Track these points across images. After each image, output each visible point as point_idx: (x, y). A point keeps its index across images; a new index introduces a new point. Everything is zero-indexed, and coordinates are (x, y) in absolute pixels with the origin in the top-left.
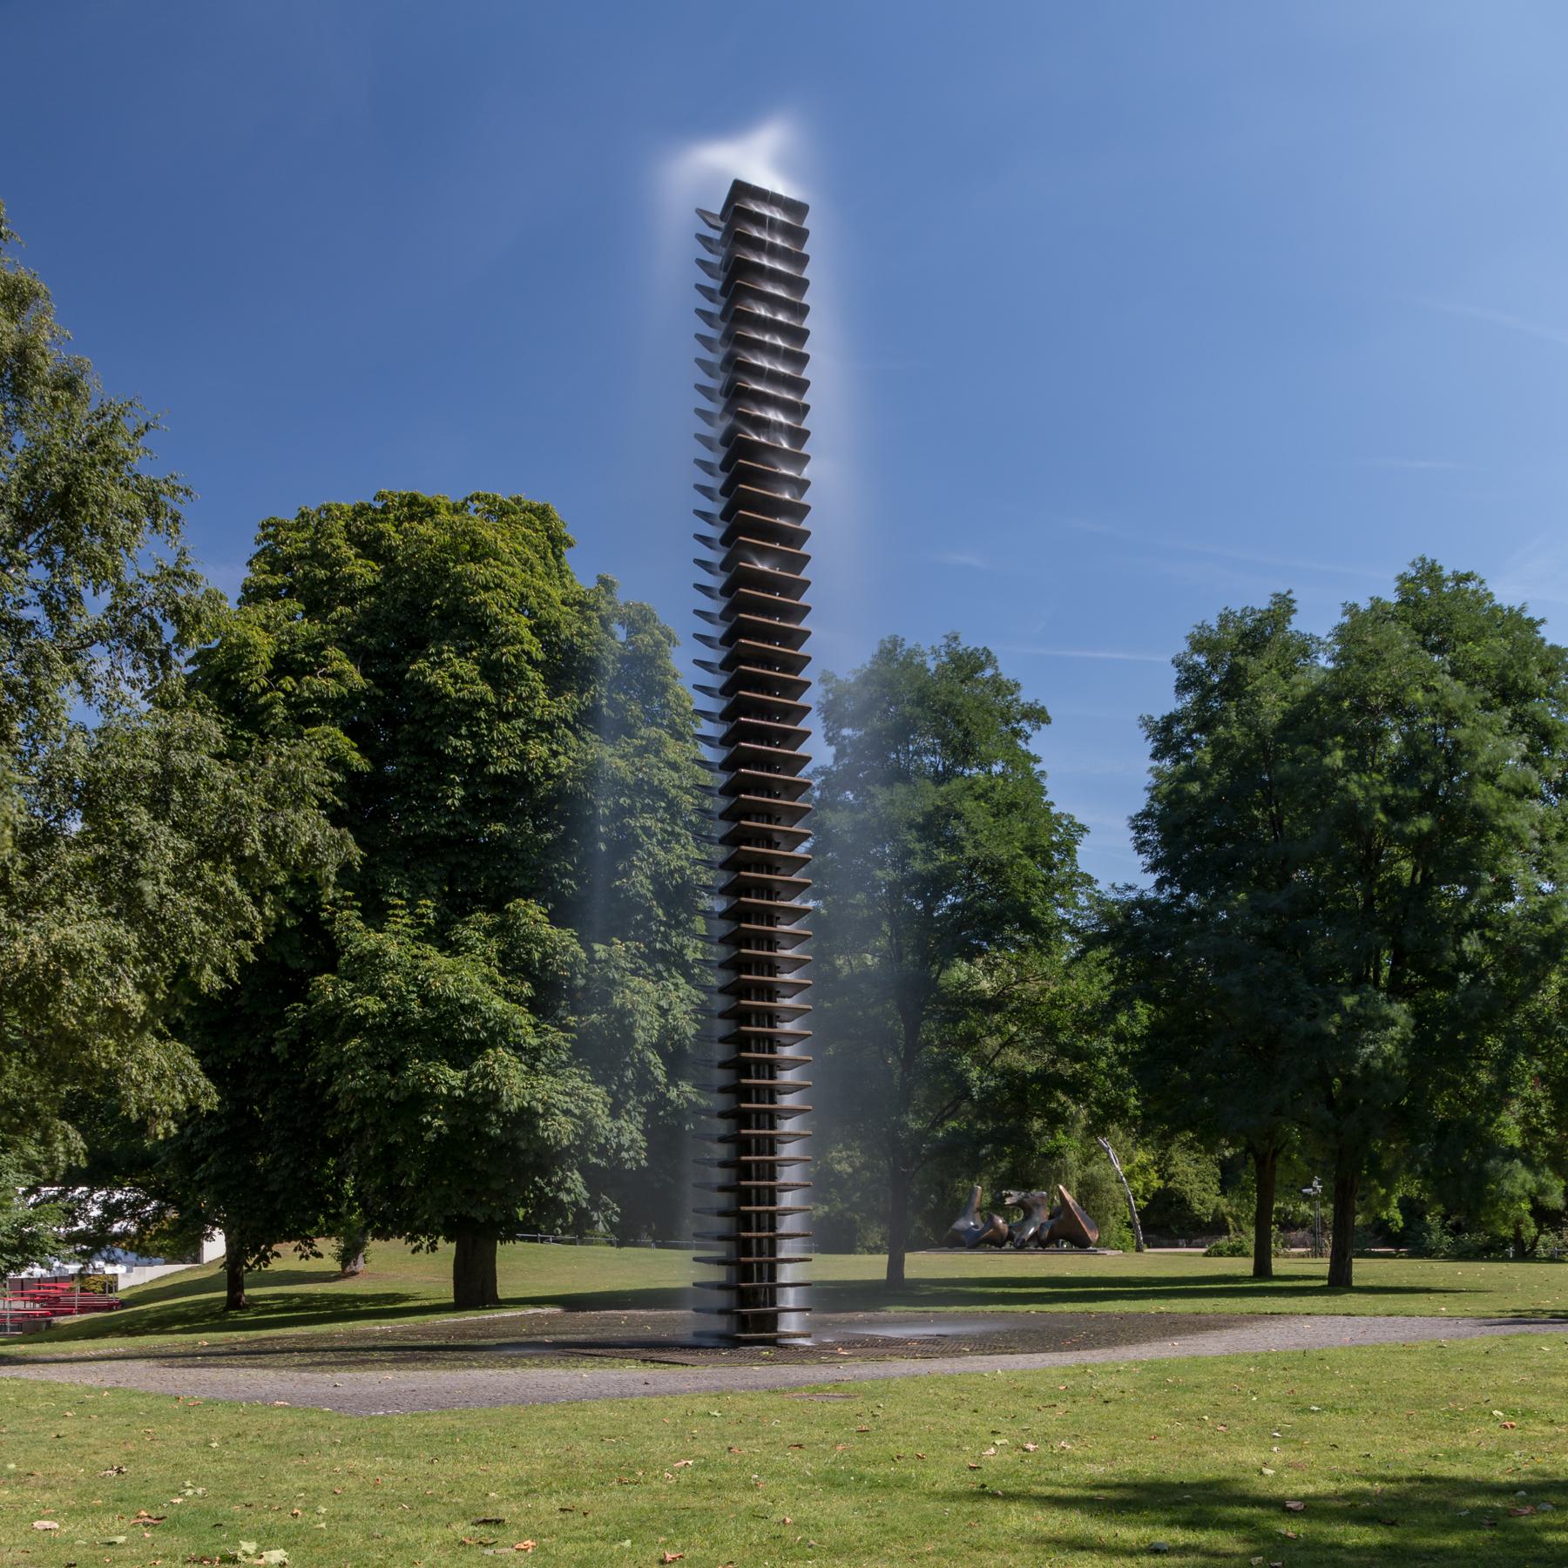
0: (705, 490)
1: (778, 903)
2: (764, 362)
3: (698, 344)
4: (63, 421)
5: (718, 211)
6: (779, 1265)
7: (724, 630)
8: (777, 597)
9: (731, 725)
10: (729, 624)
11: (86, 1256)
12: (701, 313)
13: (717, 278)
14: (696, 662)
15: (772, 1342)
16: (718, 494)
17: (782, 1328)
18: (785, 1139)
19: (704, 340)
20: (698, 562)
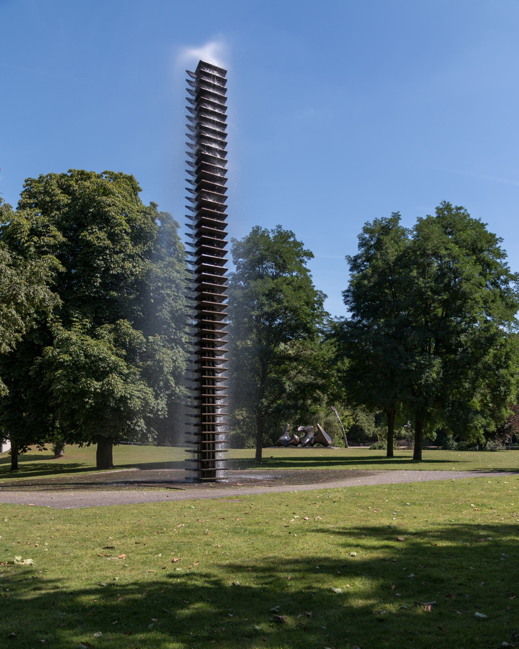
0: (189, 172)
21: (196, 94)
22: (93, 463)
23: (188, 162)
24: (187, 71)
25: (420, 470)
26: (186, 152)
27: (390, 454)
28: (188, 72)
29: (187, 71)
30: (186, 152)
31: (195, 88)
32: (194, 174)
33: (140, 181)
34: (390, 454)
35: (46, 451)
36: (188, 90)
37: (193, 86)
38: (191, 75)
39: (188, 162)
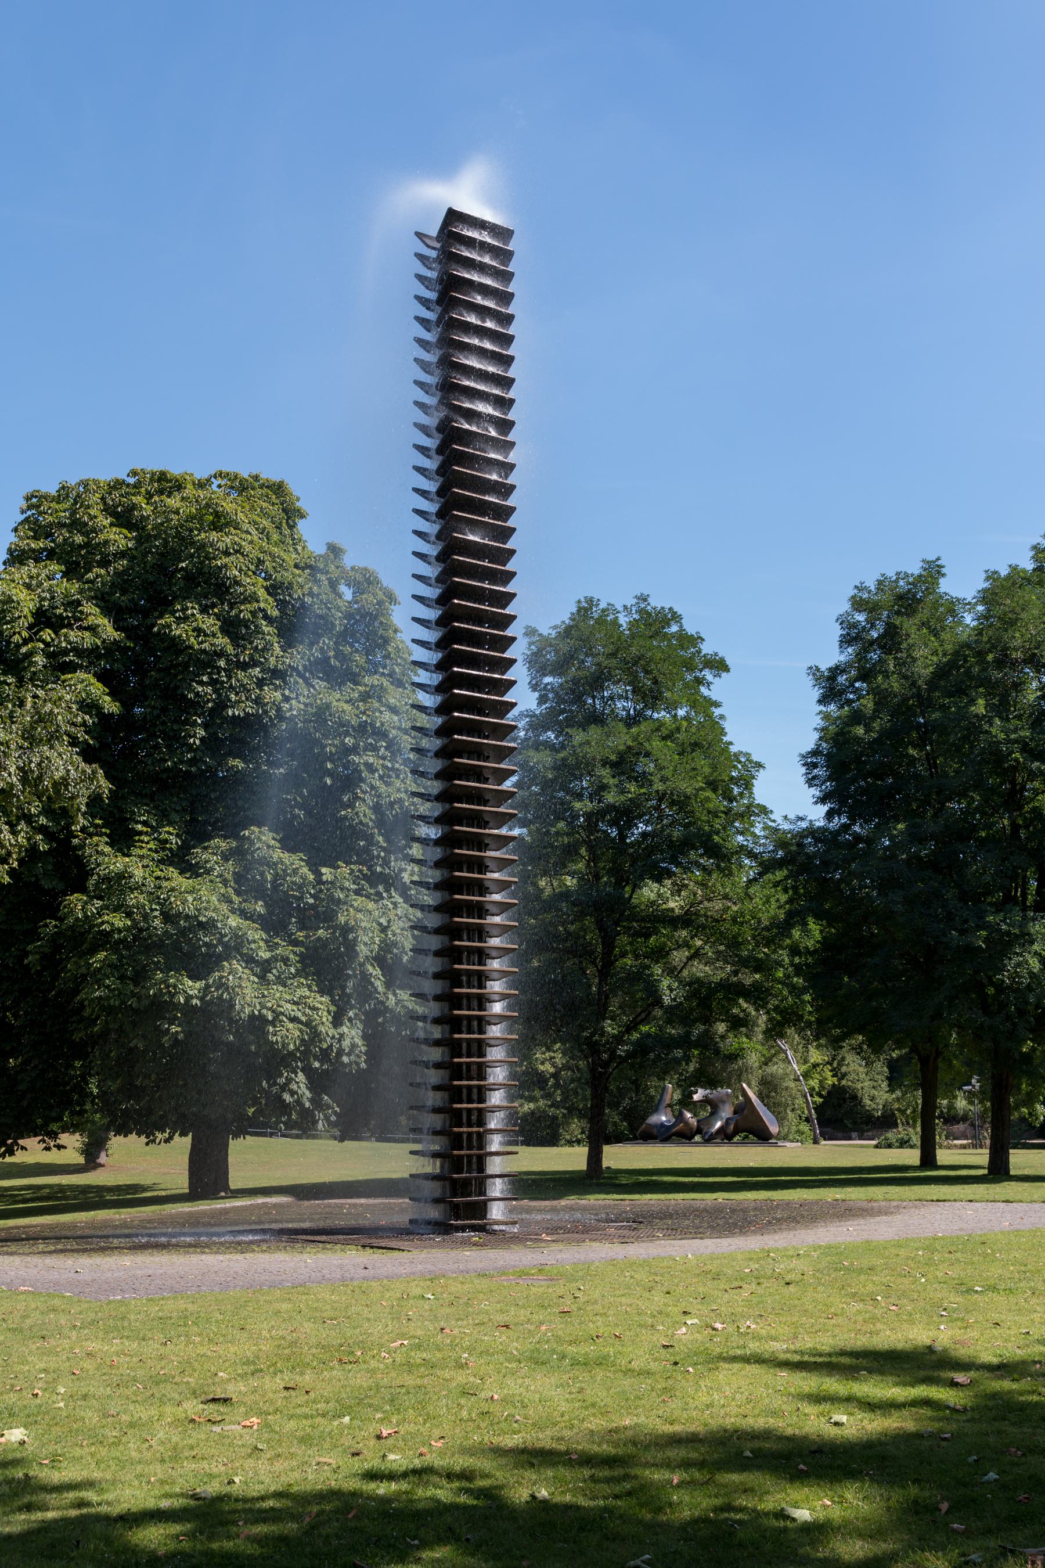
0: (423, 450)
1: (487, 831)
7: (438, 591)
18: (492, 1042)
27: (928, 1159)
28: (419, 235)
34: (928, 1159)
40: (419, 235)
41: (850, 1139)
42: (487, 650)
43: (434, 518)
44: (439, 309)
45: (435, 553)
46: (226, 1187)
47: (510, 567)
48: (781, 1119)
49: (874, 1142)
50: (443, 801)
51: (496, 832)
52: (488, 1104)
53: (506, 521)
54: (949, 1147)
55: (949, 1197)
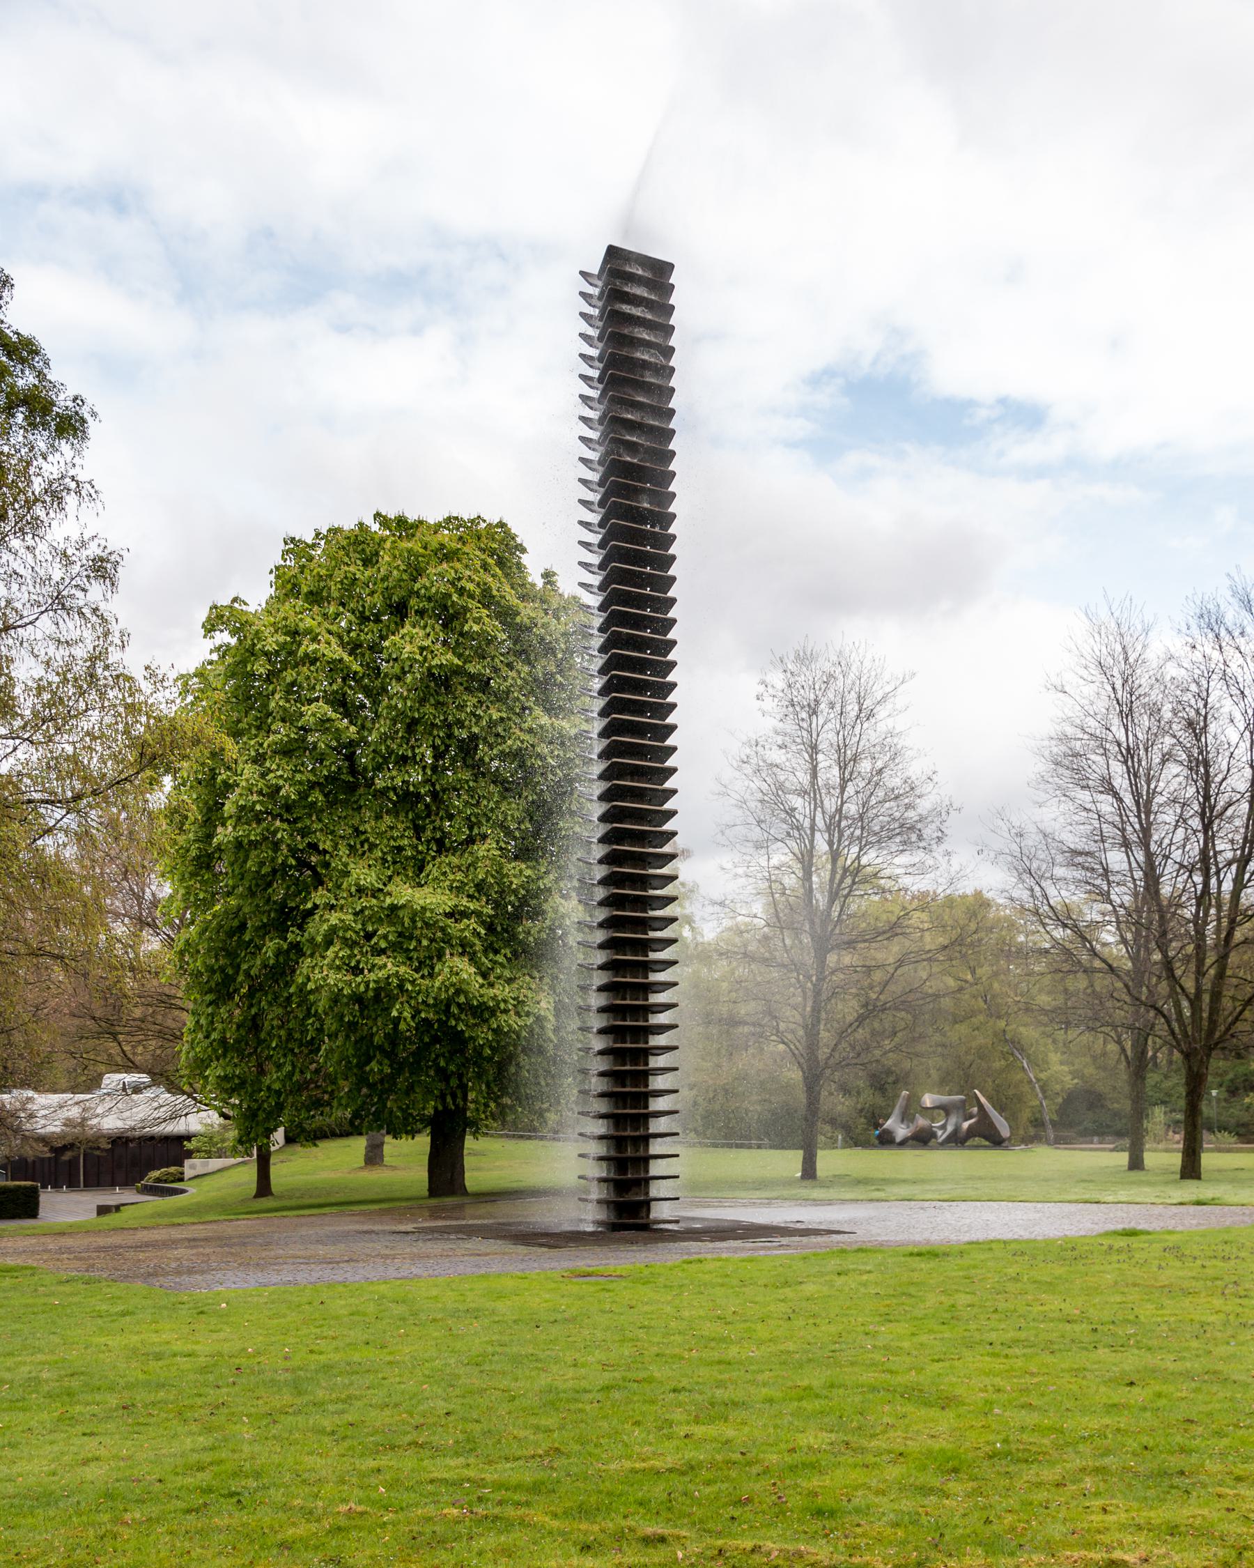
0: (585, 503)
1: (651, 850)
2: (637, 312)
3: (581, 424)
4: (279, 1465)
5: (596, 271)
6: (653, 1204)
7: (601, 599)
8: (648, 612)
9: (607, 720)
10: (607, 657)
11: (283, 932)
12: (584, 315)
13: (596, 286)
14: (580, 563)
15: (645, 1227)
16: (596, 341)
17: (653, 1215)
18: (655, 1009)
19: (585, 399)
20: (582, 460)
21: (601, 469)
22: (589, 1216)
23: (584, 482)
24: (582, 273)
25: (1199, 1203)
26: (581, 335)
27: (809, 1172)
28: (583, 274)
29: (582, 273)
30: (581, 335)
31: (598, 332)
32: (596, 507)
33: (521, 531)
34: (809, 1172)
35: (582, 1173)
36: (584, 315)
37: (594, 306)
38: (591, 280)
39: (584, 482)
40: (583, 274)
41: (1092, 1143)
42: (650, 739)
43: (596, 590)
44: (601, 345)
45: (597, 604)
46: (463, 1191)
47: (670, 720)
48: (1012, 1119)
49: (1111, 1146)
50: (608, 864)
51: (659, 871)
52: (650, 1088)
53: (665, 697)
54: (1155, 1150)
55: (1192, 1209)
